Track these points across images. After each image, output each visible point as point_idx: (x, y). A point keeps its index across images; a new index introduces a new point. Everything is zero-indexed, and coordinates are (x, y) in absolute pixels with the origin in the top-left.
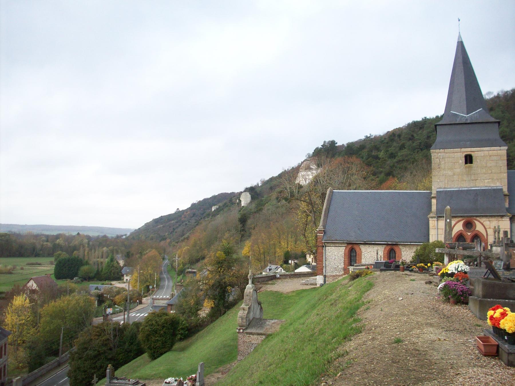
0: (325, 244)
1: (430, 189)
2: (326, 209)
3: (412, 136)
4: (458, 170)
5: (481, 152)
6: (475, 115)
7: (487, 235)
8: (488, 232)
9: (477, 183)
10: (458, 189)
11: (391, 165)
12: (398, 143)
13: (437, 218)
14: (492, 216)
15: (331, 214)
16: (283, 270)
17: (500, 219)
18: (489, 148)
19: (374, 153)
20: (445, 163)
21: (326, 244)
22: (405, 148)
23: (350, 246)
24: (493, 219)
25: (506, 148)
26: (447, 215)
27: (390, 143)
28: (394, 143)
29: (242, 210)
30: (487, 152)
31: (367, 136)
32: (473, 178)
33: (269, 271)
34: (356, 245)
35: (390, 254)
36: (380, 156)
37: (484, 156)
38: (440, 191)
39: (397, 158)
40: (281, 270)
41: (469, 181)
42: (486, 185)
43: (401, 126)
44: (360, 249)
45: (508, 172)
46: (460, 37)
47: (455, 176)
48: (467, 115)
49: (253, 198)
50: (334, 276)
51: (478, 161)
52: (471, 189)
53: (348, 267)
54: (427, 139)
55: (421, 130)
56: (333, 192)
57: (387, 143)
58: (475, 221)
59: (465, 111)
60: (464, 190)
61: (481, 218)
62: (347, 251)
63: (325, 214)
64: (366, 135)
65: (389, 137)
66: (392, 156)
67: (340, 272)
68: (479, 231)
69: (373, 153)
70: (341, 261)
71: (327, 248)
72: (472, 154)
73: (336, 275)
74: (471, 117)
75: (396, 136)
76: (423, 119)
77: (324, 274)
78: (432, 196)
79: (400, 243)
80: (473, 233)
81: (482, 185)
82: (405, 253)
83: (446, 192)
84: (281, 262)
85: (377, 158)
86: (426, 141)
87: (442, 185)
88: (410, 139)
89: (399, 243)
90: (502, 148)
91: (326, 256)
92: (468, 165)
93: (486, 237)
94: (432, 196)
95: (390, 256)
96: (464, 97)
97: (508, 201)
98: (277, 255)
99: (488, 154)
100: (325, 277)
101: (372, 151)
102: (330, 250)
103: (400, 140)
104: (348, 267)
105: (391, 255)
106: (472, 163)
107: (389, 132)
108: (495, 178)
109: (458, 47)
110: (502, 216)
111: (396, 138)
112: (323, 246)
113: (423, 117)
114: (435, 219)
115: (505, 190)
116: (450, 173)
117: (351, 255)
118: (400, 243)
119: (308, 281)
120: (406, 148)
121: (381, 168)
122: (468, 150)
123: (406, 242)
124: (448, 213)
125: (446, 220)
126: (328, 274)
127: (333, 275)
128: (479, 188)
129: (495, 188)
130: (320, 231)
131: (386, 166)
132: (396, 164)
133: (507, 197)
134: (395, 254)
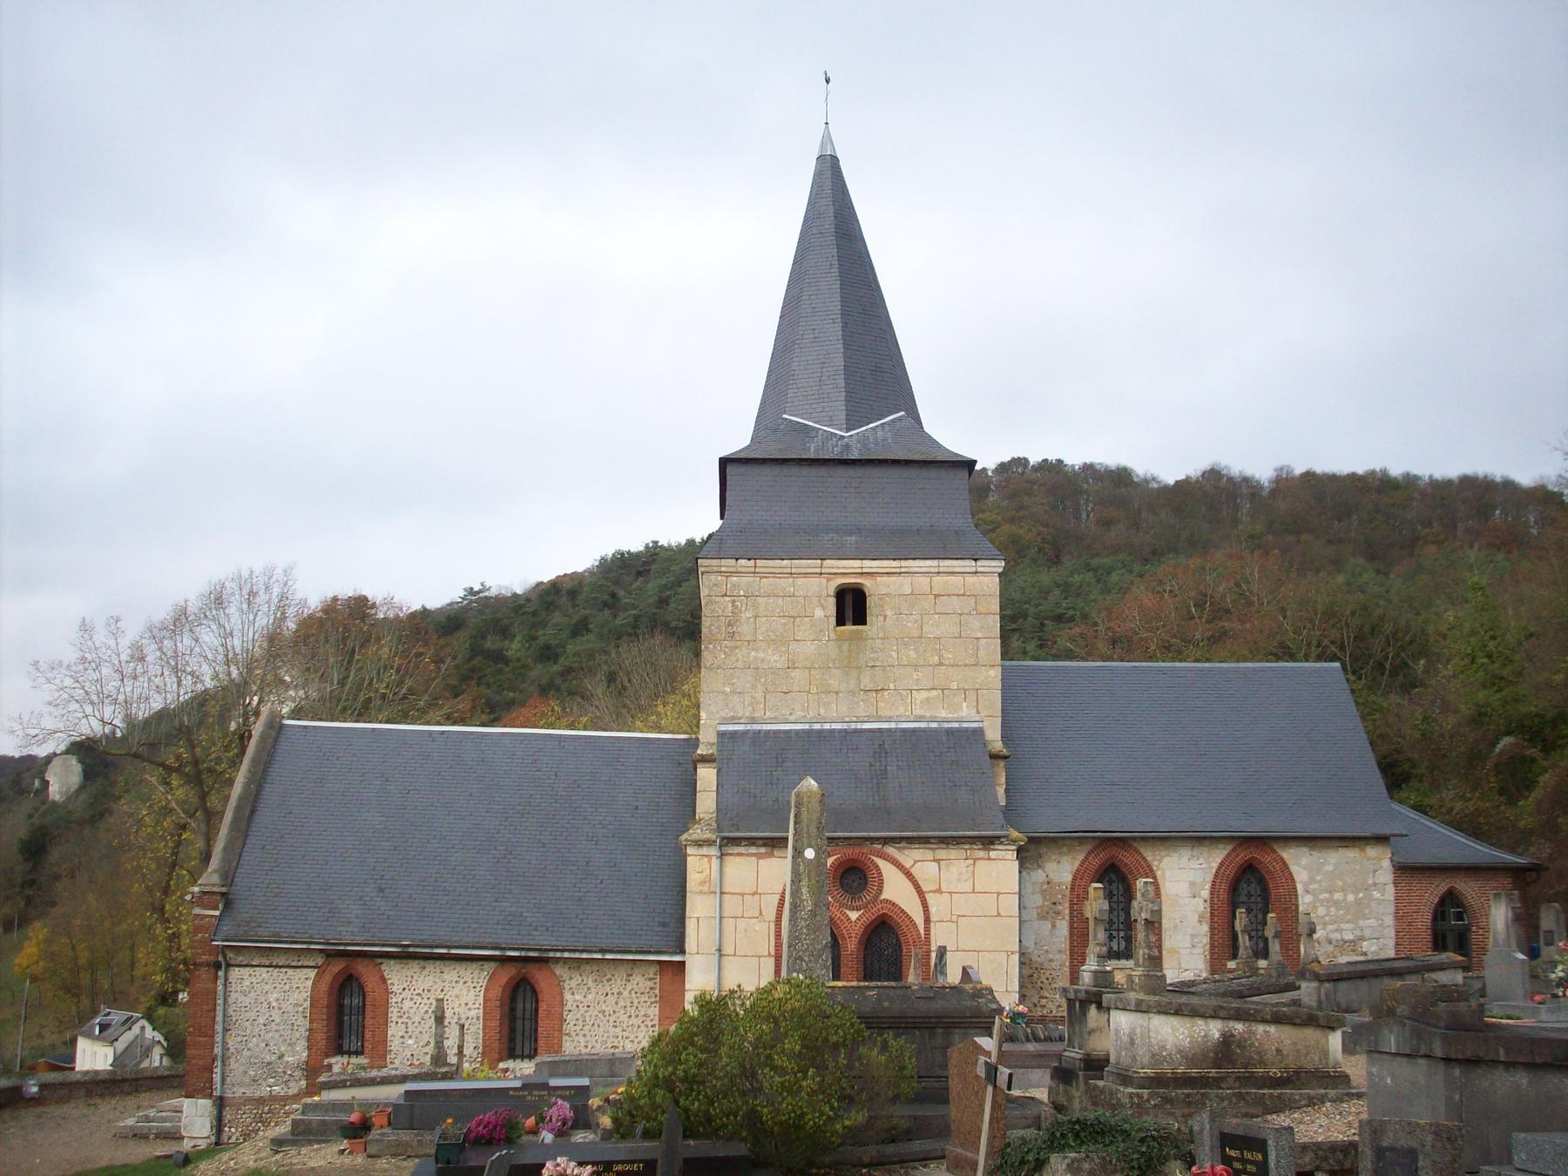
0: (225, 957)
1: (695, 724)
2: (241, 799)
3: (613, 595)
4: (809, 649)
5: (900, 579)
6: (880, 434)
7: (927, 920)
8: (933, 910)
9: (881, 704)
10: (807, 727)
11: (544, 681)
12: (566, 616)
13: (720, 847)
14: (946, 841)
15: (266, 817)
16: (149, 1028)
17: (981, 854)
18: (935, 563)
19: (490, 644)
20: (756, 617)
21: (230, 955)
22: (588, 630)
23: (337, 966)
24: (953, 853)
25: (999, 566)
26: (804, 825)
27: (544, 613)
28: (557, 613)
29: (36, 815)
30: (925, 580)
31: (472, 589)
32: (866, 682)
33: (100, 1032)
34: (366, 961)
35: (513, 1000)
36: (510, 653)
37: (912, 594)
38: (734, 733)
39: (561, 660)
40: (143, 1028)
41: (853, 693)
42: (918, 712)
43: (580, 570)
44: (384, 980)
45: (1004, 669)
46: (827, 139)
47: (795, 673)
48: (848, 430)
49: (88, 775)
50: (261, 1101)
51: (889, 613)
52: (859, 726)
53: (326, 1062)
54: (658, 608)
55: (641, 579)
56: (282, 726)
57: (534, 614)
58: (881, 863)
59: (839, 409)
60: (832, 731)
61: (904, 848)
62: (324, 987)
63: (235, 820)
64: (468, 585)
65: (541, 596)
66: (548, 654)
67: (292, 1084)
68: (894, 904)
69: (489, 643)
70: (298, 1035)
71: (235, 973)
72: (867, 583)
73: (274, 1098)
74: (862, 439)
75: (564, 592)
76: (647, 546)
77: (217, 1093)
78: (699, 752)
79: (558, 955)
80: (871, 916)
81: (901, 711)
82: (577, 997)
83: (758, 738)
84: (146, 1001)
85: (498, 657)
86: (654, 614)
87: (741, 708)
88: (606, 605)
89: (551, 954)
90: (983, 565)
91: (230, 1011)
92: (849, 628)
93: (922, 932)
94: (699, 752)
95: (513, 1010)
96: (839, 361)
97: (1003, 780)
98: (138, 973)
99: (926, 589)
100: (221, 1103)
101: (484, 637)
102: (247, 983)
103: (575, 606)
104: (326, 1062)
105: (520, 1006)
106: (864, 623)
107: (542, 583)
108: (954, 686)
109: (818, 175)
110: (988, 842)
111: (564, 600)
112: (218, 966)
113: (649, 540)
114: (714, 851)
115: (994, 734)
116: (776, 657)
117: (341, 1006)
118: (558, 955)
119: (147, 1119)
120: (591, 632)
121: (511, 689)
122: (848, 570)
123: (583, 951)
124: (811, 812)
125: (798, 853)
126: (236, 1092)
127: (258, 1094)
128: (893, 725)
129: (956, 725)
130: (204, 899)
131: (525, 685)
132: (558, 681)
133: (1002, 764)
134: (537, 1001)
